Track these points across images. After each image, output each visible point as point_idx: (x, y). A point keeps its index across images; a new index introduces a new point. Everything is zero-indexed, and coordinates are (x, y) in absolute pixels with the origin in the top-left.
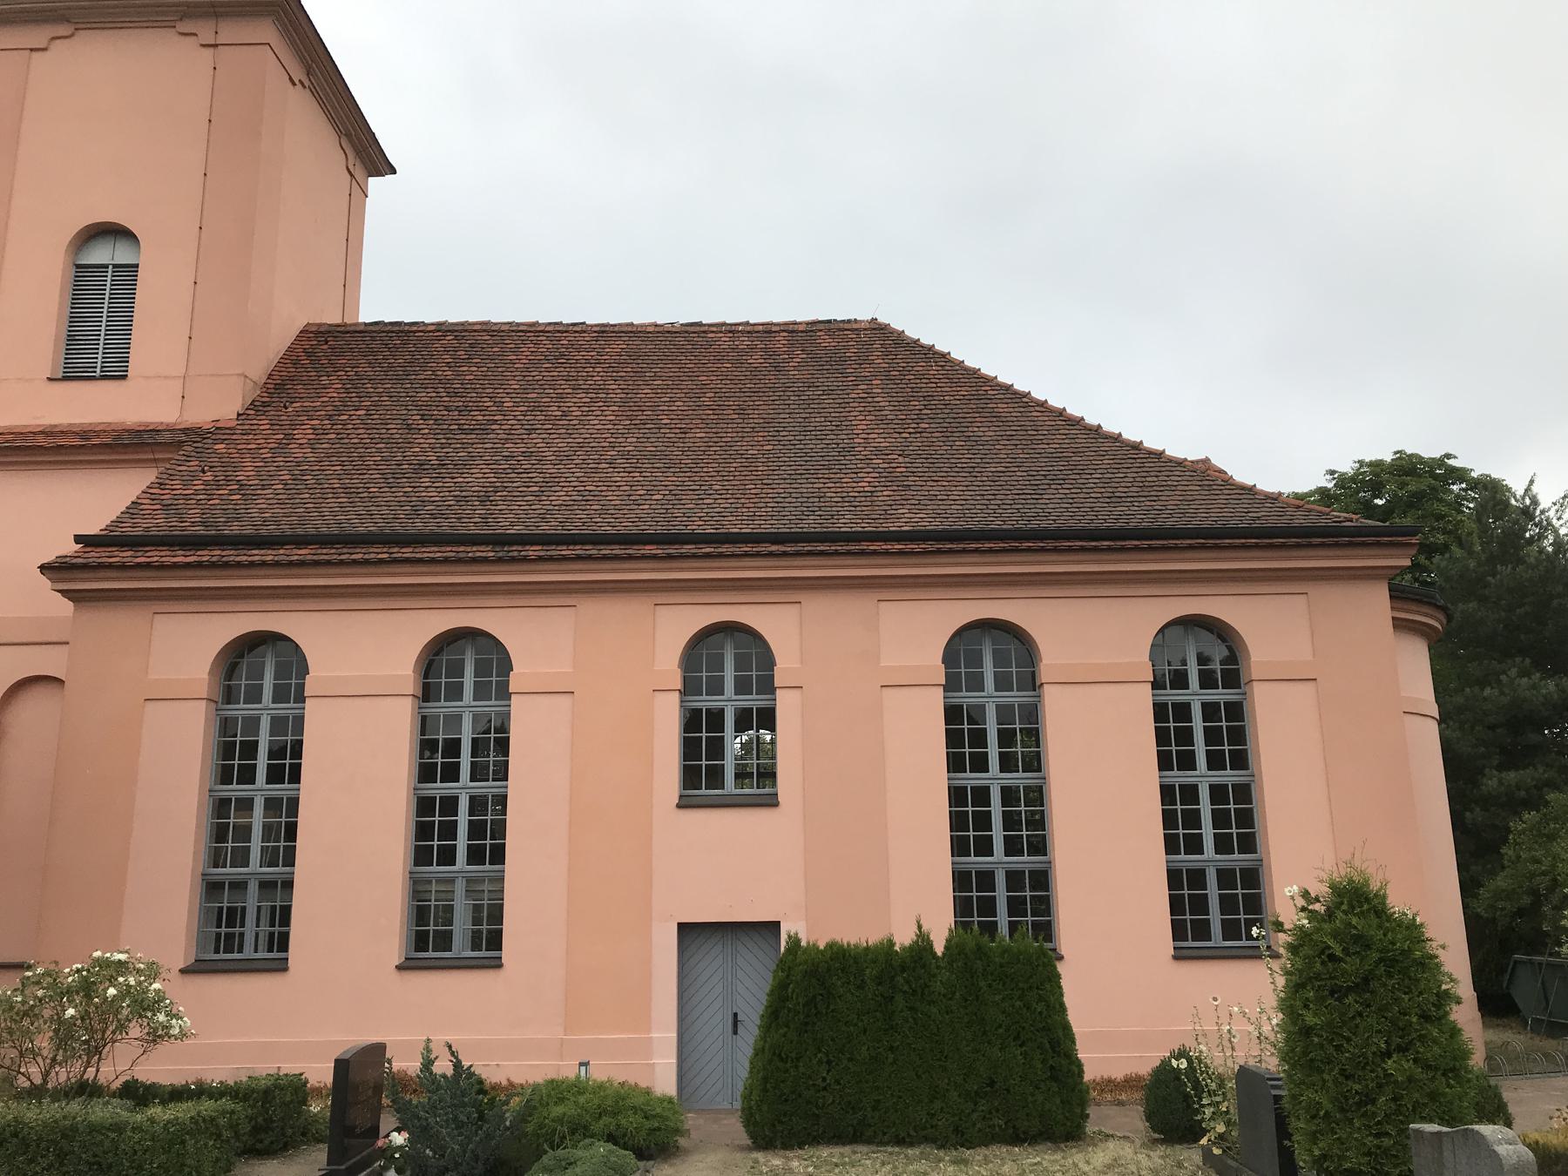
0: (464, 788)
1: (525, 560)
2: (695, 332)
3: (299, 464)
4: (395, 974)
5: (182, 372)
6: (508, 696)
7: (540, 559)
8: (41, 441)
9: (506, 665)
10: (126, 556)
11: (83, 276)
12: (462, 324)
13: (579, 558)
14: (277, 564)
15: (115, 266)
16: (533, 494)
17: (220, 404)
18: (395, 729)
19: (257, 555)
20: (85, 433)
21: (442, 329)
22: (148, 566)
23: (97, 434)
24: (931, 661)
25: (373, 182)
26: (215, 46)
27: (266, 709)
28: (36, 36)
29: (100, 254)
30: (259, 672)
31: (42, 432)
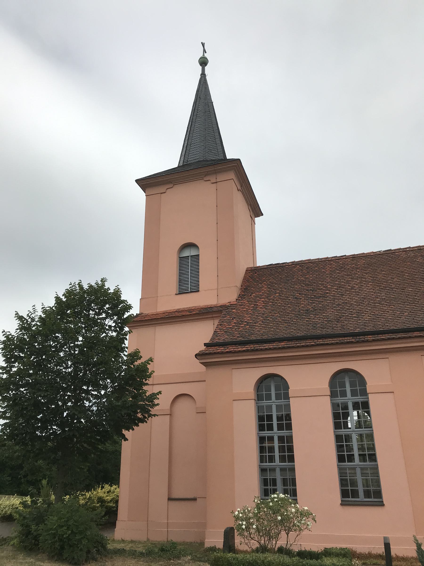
0: (276, 433)
1: (368, 341)
2: (389, 253)
3: (263, 314)
4: (341, 508)
5: (217, 288)
6: (288, 398)
7: (374, 341)
8: (177, 314)
9: (286, 387)
10: (221, 349)
11: (182, 260)
12: (301, 261)
13: (389, 339)
14: (275, 349)
15: (191, 256)
16: (355, 317)
17: (230, 296)
18: (324, 408)
19: (267, 346)
20: (190, 310)
21: (294, 264)
22: (230, 352)
23: (193, 310)
24: (324, 385)
25: (257, 219)
26: (216, 182)
27: (274, 402)
28: (162, 189)
29: (187, 253)
30: (271, 388)
31: (176, 311)
